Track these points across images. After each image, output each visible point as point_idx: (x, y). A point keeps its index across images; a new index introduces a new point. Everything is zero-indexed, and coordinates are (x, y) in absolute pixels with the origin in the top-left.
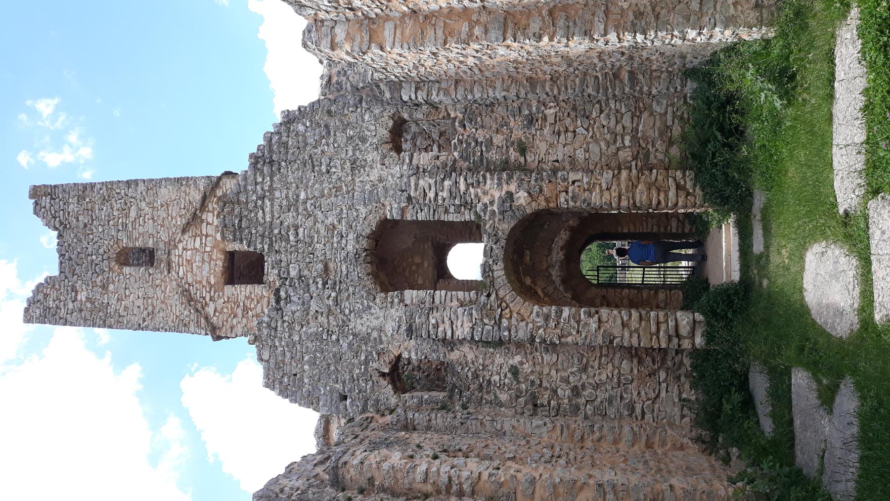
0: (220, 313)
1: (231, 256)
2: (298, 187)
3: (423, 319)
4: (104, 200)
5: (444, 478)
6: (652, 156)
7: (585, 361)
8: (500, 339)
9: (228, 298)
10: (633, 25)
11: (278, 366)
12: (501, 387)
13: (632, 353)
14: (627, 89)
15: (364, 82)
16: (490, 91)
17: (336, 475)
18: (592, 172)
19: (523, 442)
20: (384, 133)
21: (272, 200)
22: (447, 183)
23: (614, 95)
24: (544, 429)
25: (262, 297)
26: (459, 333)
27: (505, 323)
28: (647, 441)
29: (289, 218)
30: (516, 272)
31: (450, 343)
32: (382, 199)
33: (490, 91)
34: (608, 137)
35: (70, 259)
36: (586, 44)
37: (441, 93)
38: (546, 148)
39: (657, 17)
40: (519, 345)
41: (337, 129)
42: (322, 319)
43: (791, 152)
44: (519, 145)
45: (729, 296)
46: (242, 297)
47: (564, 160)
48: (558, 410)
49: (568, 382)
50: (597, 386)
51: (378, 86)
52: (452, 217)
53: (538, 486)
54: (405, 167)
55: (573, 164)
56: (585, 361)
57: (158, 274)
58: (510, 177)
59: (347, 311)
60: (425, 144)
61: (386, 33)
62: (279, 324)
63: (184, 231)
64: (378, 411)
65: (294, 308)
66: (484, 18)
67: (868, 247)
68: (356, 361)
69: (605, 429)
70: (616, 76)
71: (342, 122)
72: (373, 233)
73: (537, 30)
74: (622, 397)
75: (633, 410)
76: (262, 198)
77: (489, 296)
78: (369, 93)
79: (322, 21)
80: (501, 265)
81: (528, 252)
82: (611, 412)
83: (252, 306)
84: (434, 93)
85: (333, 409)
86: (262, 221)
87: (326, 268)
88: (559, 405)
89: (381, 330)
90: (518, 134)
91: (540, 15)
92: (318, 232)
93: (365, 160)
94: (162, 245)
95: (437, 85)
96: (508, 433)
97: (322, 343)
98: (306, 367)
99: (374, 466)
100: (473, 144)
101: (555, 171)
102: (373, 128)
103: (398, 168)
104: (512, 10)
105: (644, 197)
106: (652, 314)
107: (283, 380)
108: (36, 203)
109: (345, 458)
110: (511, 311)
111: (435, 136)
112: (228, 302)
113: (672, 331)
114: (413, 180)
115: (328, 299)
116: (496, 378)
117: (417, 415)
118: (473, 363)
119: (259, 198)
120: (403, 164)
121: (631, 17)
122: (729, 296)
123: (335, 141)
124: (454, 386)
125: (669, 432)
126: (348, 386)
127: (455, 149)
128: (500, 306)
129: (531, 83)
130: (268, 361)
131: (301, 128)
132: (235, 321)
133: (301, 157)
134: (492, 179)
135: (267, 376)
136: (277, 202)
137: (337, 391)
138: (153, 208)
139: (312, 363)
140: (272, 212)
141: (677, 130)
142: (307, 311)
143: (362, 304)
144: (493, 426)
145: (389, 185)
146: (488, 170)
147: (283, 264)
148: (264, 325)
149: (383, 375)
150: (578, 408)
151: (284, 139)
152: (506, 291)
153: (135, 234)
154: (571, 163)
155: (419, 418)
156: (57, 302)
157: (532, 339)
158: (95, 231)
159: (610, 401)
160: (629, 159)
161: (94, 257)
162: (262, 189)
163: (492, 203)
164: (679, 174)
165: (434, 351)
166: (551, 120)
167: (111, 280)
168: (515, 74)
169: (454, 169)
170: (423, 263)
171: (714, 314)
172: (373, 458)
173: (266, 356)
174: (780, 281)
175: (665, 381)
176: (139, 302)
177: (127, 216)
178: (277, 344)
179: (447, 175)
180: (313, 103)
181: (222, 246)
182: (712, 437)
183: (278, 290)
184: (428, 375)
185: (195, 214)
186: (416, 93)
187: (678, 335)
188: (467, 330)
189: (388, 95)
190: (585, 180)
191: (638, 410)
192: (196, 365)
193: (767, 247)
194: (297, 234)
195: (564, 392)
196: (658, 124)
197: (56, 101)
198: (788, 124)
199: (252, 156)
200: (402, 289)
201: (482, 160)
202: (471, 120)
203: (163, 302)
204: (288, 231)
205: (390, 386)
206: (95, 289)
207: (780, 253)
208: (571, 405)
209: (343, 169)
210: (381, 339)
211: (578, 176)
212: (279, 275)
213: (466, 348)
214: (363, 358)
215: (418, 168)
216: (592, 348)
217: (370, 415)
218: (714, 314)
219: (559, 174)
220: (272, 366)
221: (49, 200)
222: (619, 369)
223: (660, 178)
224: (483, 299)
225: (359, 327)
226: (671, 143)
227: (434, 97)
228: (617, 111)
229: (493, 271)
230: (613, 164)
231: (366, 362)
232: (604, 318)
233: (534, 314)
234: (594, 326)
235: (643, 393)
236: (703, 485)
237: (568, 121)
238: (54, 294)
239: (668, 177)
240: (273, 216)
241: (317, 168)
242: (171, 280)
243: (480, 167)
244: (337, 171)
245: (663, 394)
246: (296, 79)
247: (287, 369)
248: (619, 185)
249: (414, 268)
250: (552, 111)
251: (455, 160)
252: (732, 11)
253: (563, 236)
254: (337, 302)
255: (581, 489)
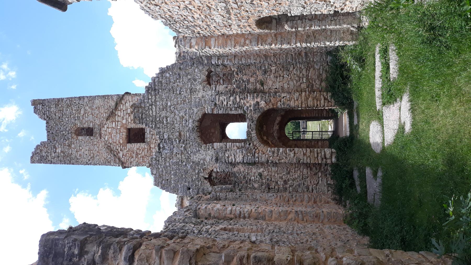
0: (125, 156)
2: (167, 100)
3: (223, 154)
4: (68, 106)
6: (314, 86)
8: (255, 162)
9: (129, 149)
10: (306, 40)
11: (160, 176)
12: (255, 182)
13: (308, 166)
14: (304, 60)
15: (196, 56)
16: (249, 60)
17: (196, 213)
18: (291, 93)
19: (265, 203)
20: (204, 77)
21: (156, 106)
22: (231, 98)
24: (273, 197)
25: (145, 148)
26: (238, 160)
27: (256, 155)
28: (314, 201)
29: (163, 114)
31: (234, 164)
32: (204, 105)
33: (249, 60)
34: (297, 78)
35: (52, 133)
36: (288, 46)
37: (229, 61)
38: (272, 83)
39: (315, 38)
40: (262, 164)
41: (183, 75)
42: (179, 156)
43: (364, 87)
44: (261, 82)
45: (345, 142)
46: (135, 149)
48: (278, 190)
50: (294, 180)
52: (233, 112)
54: (213, 91)
58: (258, 96)
59: (190, 152)
60: (217, 79)
61: (212, 42)
62: (160, 159)
63: (107, 120)
64: (204, 194)
65: (166, 152)
66: (250, 37)
67: (383, 122)
68: (194, 173)
70: (300, 54)
71: (185, 72)
72: (200, 119)
74: (304, 184)
75: (308, 189)
76: (152, 105)
77: (250, 144)
78: (197, 60)
79: (186, 37)
80: (254, 131)
81: (265, 126)
82: (300, 190)
83: (140, 153)
84: (226, 61)
85: (184, 193)
86: (152, 115)
87: (180, 135)
88: (279, 188)
89: (204, 160)
90: (260, 78)
91: (271, 36)
92: (176, 119)
93: (196, 89)
94: (97, 126)
96: (259, 199)
97: (179, 166)
98: (172, 176)
101: (276, 93)
102: (199, 75)
103: (210, 92)
105: (312, 103)
106: (315, 150)
107: (162, 182)
108: (35, 108)
109: (199, 207)
110: (259, 150)
111: (221, 76)
112: (129, 151)
113: (323, 157)
114: (217, 97)
115: (181, 147)
116: (253, 178)
117: (221, 194)
118: (243, 172)
119: (150, 105)
121: (305, 37)
122: (345, 142)
123: (183, 81)
124: (236, 182)
125: (323, 197)
126: (191, 184)
127: (234, 84)
128: (254, 148)
130: (155, 174)
131: (168, 75)
132: (132, 160)
133: (168, 87)
134: (250, 96)
135: (155, 181)
137: (186, 186)
138: (92, 109)
139: (175, 175)
141: (324, 76)
142: (172, 152)
143: (196, 149)
144: (252, 197)
145: (206, 98)
146: (248, 92)
147: (161, 133)
148: (154, 159)
149: (206, 178)
150: (286, 189)
152: (256, 142)
153: (84, 121)
154: (282, 89)
155: (222, 195)
156: (47, 153)
157: (268, 161)
159: (299, 185)
160: (305, 87)
161: (64, 132)
162: (151, 101)
163: (250, 106)
164: (325, 94)
165: (227, 168)
166: (273, 71)
168: (259, 53)
169: (234, 92)
170: (215, 132)
171: (340, 149)
173: (155, 172)
174: (363, 135)
176: (87, 152)
177: (80, 113)
178: (159, 167)
180: (173, 64)
181: (125, 126)
183: (159, 144)
184: (220, 181)
185: (112, 112)
186: (218, 61)
187: (325, 158)
189: (206, 62)
190: (288, 96)
191: (310, 189)
192: (77, 190)
193: (358, 122)
194: (167, 120)
195: (281, 183)
196: (317, 73)
198: (364, 77)
199: (146, 87)
201: (245, 88)
203: (98, 152)
204: (163, 119)
207: (362, 124)
209: (186, 92)
210: (204, 164)
211: (285, 95)
212: (160, 138)
213: (240, 166)
214: (197, 172)
215: (219, 92)
216: (292, 164)
217: (201, 195)
218: (340, 149)
220: (158, 176)
221: (41, 107)
223: (317, 95)
224: (247, 145)
225: (195, 159)
226: (322, 81)
228: (300, 68)
229: (251, 134)
230: (299, 90)
231: (198, 174)
232: (296, 152)
233: (268, 151)
234: (292, 155)
235: (312, 182)
237: (280, 72)
239: (321, 95)
240: (156, 113)
243: (245, 91)
244: (184, 93)
245: (320, 182)
249: (211, 134)
250: (274, 68)
251: (234, 88)
253: (279, 119)
254: (185, 148)
255: (289, 213)
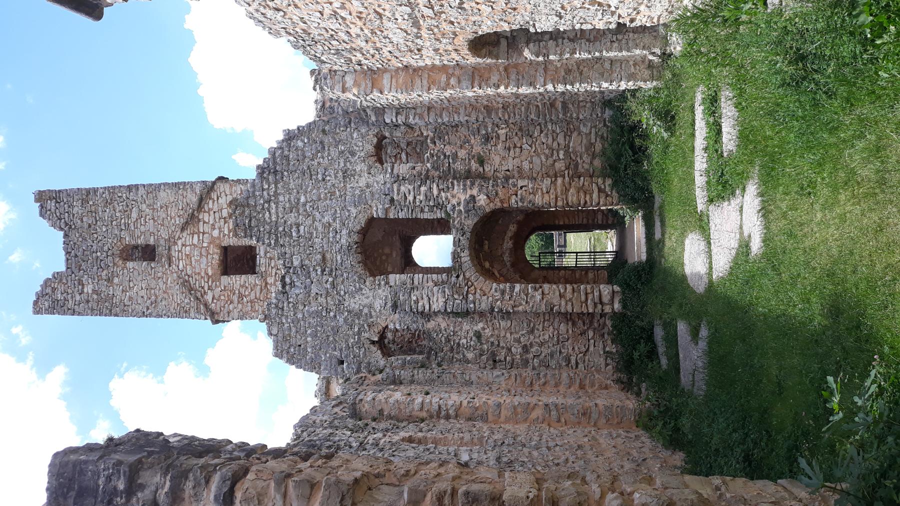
0: (218, 300)
1: (225, 250)
3: (406, 297)
5: (436, 407)
7: (532, 325)
10: (565, 79)
11: (285, 339)
12: (468, 348)
13: (568, 317)
14: (561, 116)
15: (354, 107)
17: (355, 409)
19: (487, 388)
20: (370, 148)
21: (277, 203)
22: (423, 189)
23: (551, 120)
24: (502, 378)
25: (256, 285)
26: (435, 307)
27: (471, 297)
29: (292, 218)
30: (478, 257)
31: (427, 316)
32: (369, 202)
34: (547, 151)
35: (76, 256)
37: (417, 117)
38: (500, 160)
39: (581, 74)
40: (482, 314)
42: (322, 300)
44: (478, 159)
47: (513, 170)
48: (512, 364)
49: (519, 341)
50: (541, 345)
51: (365, 111)
52: (427, 216)
53: (503, 408)
54: (388, 176)
55: (521, 174)
56: (532, 325)
57: (158, 268)
58: (473, 184)
59: (342, 293)
60: (395, 152)
62: (285, 305)
63: (183, 230)
64: (370, 372)
65: (297, 291)
66: (457, 72)
68: (351, 333)
69: (549, 376)
70: (552, 105)
71: (334, 139)
73: (496, 82)
74: (560, 352)
75: (569, 361)
76: (269, 202)
77: (458, 277)
78: (357, 116)
79: (335, 71)
80: (467, 252)
81: (486, 242)
82: (553, 364)
83: (247, 293)
84: (411, 117)
85: (333, 372)
87: (324, 258)
88: (513, 360)
89: (370, 307)
90: (477, 149)
92: (316, 229)
94: (162, 242)
95: (413, 111)
96: (475, 382)
97: (322, 319)
98: (309, 339)
99: (383, 401)
100: (442, 157)
101: (507, 178)
102: (361, 144)
104: (478, 67)
106: (582, 287)
107: (289, 350)
108: (42, 207)
109: (360, 397)
111: (403, 146)
112: (225, 290)
113: (597, 300)
114: (395, 186)
115: (326, 282)
116: (464, 341)
119: (265, 202)
120: (386, 173)
121: (563, 73)
122: (638, 271)
123: (329, 155)
127: (428, 161)
129: (487, 111)
131: (300, 144)
132: (231, 307)
134: (459, 185)
135: (276, 347)
136: (281, 205)
137: (336, 357)
138: (154, 209)
139: (314, 335)
140: (277, 213)
141: (598, 147)
143: (355, 287)
144: (462, 378)
145: (374, 188)
149: (373, 343)
151: (286, 153)
152: (470, 272)
153: (137, 233)
154: (519, 172)
155: (405, 374)
156: (65, 295)
157: (492, 309)
158: (99, 230)
159: (552, 355)
160: (563, 168)
161: (99, 254)
162: (268, 194)
163: (459, 204)
164: (600, 181)
165: (414, 322)
166: (503, 138)
167: (115, 274)
168: (475, 104)
172: (381, 396)
173: (275, 331)
174: (671, 259)
175: (593, 338)
176: (143, 293)
177: (129, 217)
178: (284, 321)
179: (423, 183)
180: (310, 123)
181: (218, 242)
182: (628, 379)
183: (283, 277)
184: (402, 347)
185: (193, 214)
187: (601, 303)
188: (441, 304)
189: (373, 118)
190: (530, 186)
191: (573, 362)
192: (125, 365)
193: (663, 235)
194: (299, 231)
195: (517, 350)
196: (584, 141)
197: (234, 157)
199: (258, 167)
200: (386, 273)
201: (449, 170)
202: (440, 138)
203: (165, 292)
205: (379, 352)
206: (100, 282)
207: (670, 239)
208: (522, 360)
209: (336, 177)
210: (371, 314)
211: (525, 182)
212: (284, 265)
213: (440, 319)
214: (356, 330)
215: (398, 176)
216: (537, 315)
217: (364, 375)
218: (628, 285)
219: (511, 181)
221: (53, 204)
222: (558, 330)
224: (453, 279)
225: (353, 305)
226: (594, 156)
227: (411, 120)
228: (554, 131)
230: (551, 173)
231: (359, 333)
232: (546, 292)
233: (493, 290)
234: (539, 297)
235: (576, 348)
236: (618, 403)
238: (61, 288)
239: (592, 182)
240: (278, 216)
241: (314, 177)
242: (172, 273)
243: (448, 176)
244: (331, 179)
245: (592, 348)
246: (295, 103)
247: (293, 341)
248: (555, 189)
249: (384, 258)
250: (504, 131)
251: (428, 170)
252: (633, 70)
253: (513, 228)
254: (333, 285)
255: (533, 409)
